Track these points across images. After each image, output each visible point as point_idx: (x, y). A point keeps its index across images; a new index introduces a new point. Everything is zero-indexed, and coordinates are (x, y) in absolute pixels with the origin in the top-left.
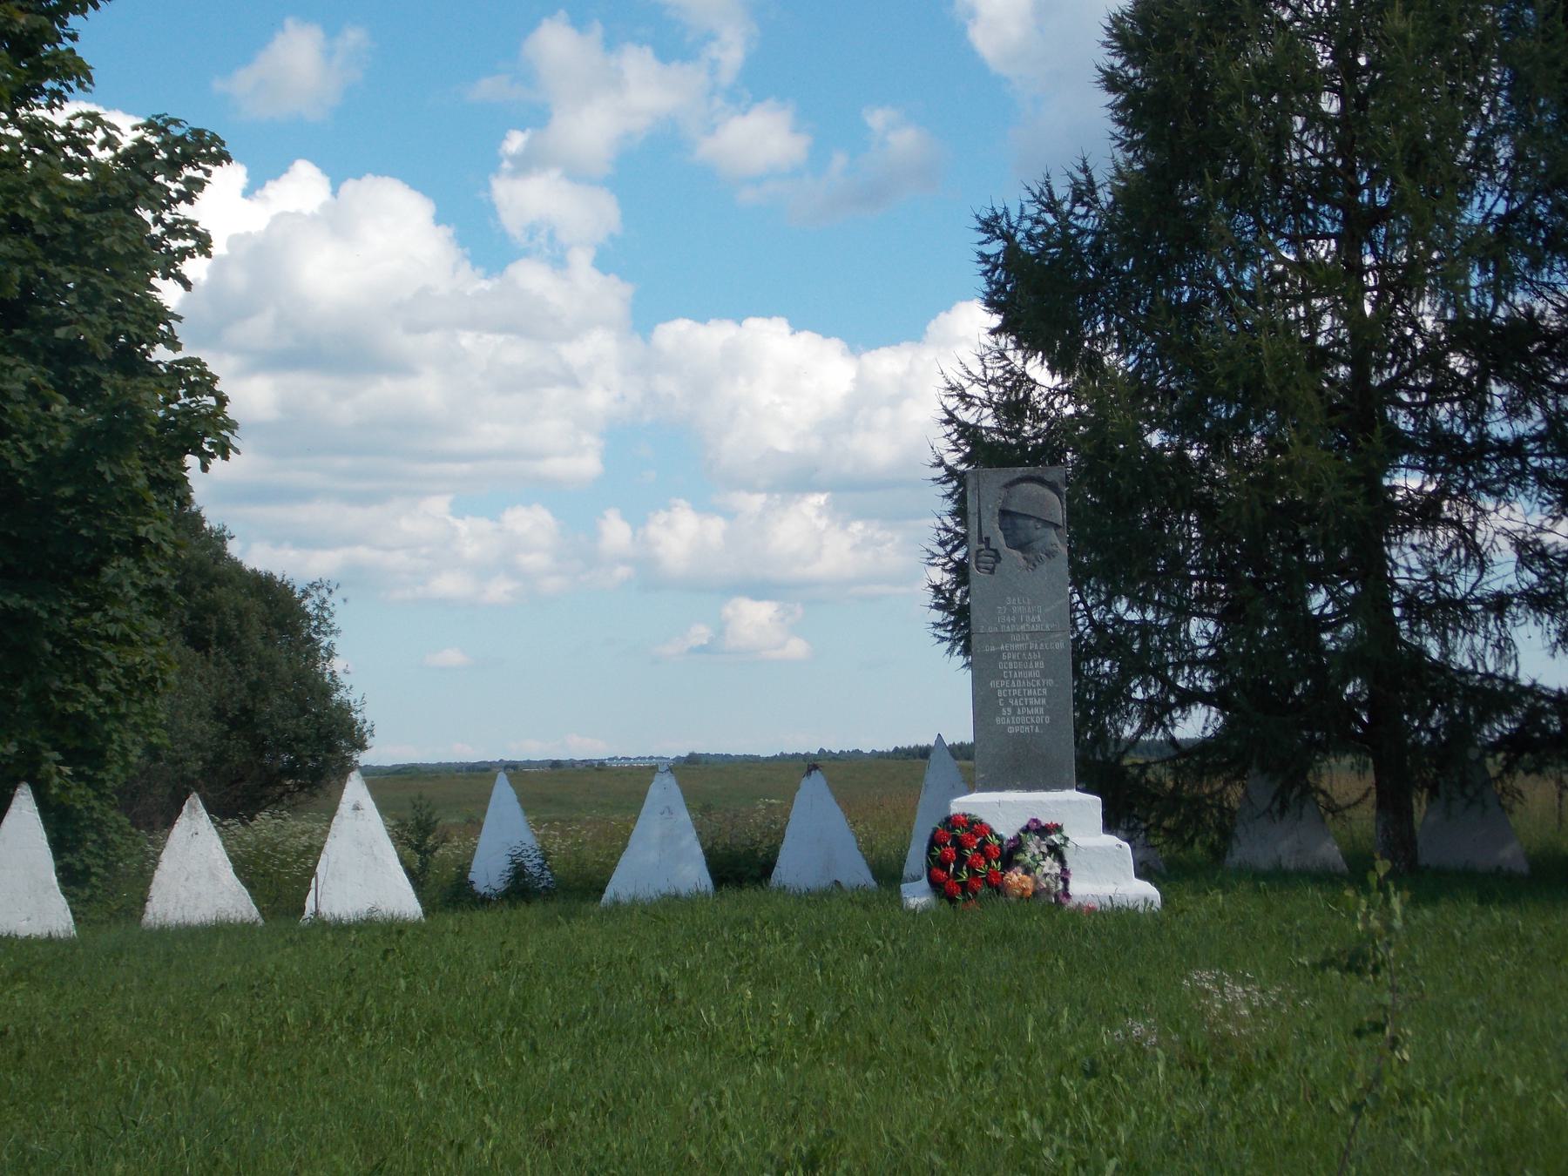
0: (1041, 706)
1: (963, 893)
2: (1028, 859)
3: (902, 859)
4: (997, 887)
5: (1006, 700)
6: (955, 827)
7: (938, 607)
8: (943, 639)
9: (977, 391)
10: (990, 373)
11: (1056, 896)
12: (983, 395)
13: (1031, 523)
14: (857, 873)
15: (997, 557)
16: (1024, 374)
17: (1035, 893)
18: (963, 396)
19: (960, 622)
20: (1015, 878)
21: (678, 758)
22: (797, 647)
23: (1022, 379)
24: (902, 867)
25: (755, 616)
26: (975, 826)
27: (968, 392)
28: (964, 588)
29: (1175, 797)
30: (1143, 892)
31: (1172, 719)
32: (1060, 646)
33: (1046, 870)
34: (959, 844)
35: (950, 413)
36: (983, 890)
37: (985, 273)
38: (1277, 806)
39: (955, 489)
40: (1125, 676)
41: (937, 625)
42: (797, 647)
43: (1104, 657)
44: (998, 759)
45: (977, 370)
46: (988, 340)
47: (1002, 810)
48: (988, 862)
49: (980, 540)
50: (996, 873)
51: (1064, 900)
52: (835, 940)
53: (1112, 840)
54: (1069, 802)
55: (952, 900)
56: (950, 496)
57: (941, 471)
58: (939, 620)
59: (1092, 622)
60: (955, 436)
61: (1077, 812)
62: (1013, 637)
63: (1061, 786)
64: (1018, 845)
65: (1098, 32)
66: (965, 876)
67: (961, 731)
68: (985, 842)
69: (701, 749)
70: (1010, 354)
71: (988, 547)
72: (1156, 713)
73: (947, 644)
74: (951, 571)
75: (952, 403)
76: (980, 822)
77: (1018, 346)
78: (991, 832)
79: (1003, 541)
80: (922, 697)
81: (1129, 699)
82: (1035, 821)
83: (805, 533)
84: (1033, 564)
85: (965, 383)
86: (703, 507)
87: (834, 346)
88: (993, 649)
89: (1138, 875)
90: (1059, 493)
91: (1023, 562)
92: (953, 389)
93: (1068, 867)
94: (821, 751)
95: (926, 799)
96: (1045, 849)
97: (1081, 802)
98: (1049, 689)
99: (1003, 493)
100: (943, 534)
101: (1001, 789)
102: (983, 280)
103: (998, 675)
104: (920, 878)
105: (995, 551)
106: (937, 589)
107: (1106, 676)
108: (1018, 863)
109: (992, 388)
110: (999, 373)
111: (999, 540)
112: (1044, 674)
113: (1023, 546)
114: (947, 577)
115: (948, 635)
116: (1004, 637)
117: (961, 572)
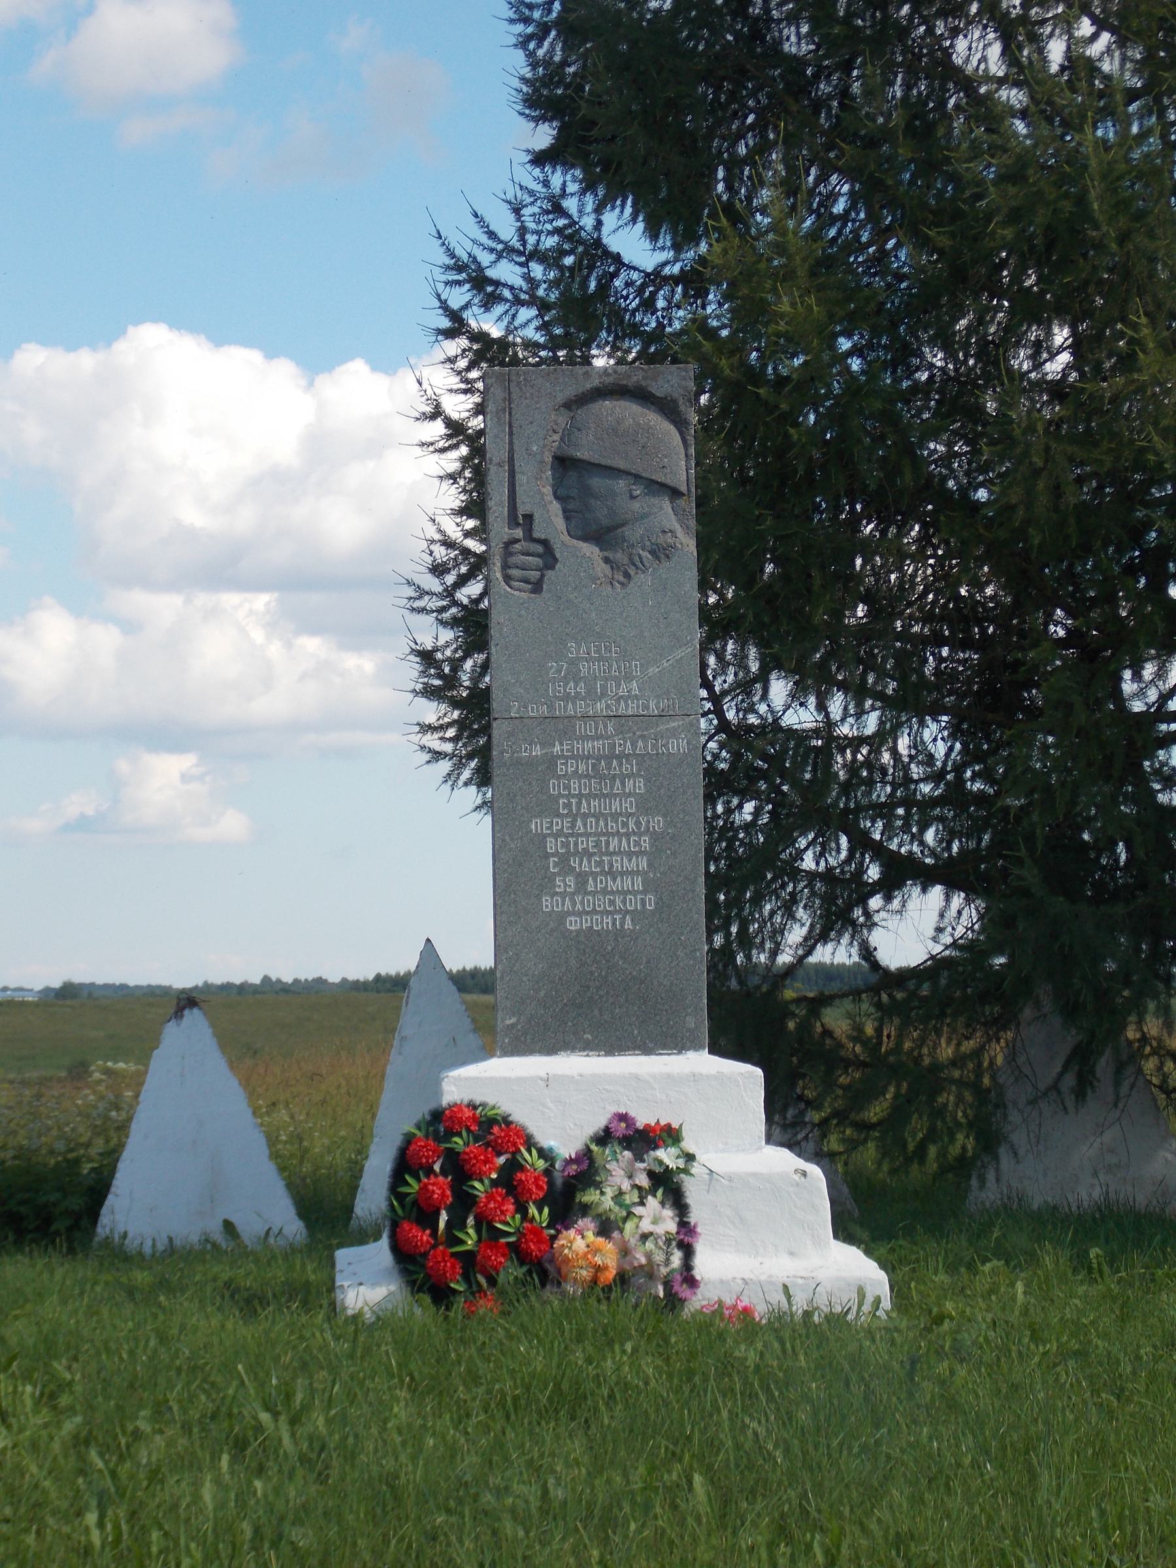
0: (635, 871)
1: (467, 1278)
2: (607, 1202)
3: (356, 1172)
4: (543, 1269)
5: (564, 860)
6: (451, 1133)
7: (429, 692)
8: (437, 756)
9: (508, 272)
10: (531, 239)
11: (667, 1284)
12: (519, 282)
13: (621, 484)
14: (270, 1212)
15: (549, 556)
16: (598, 243)
17: (623, 1278)
18: (480, 281)
19: (473, 721)
20: (580, 1244)
21: (47, 990)
22: (232, 824)
23: (596, 252)
24: (353, 1189)
25: (165, 777)
26: (494, 1131)
27: (491, 273)
28: (480, 658)
29: (879, 1065)
30: (845, 1273)
31: (868, 915)
32: (678, 746)
33: (646, 1226)
34: (460, 1170)
35: (456, 317)
36: (510, 1272)
37: (523, 42)
38: (1070, 1081)
39: (465, 460)
40: (782, 830)
41: (426, 728)
42: (232, 824)
43: (744, 795)
44: (552, 989)
45: (507, 229)
46: (530, 177)
47: (553, 1095)
48: (522, 1209)
49: (513, 521)
50: (537, 1232)
51: (683, 1291)
52: (160, 1410)
53: (783, 1160)
54: (695, 1077)
55: (441, 1295)
56: (453, 477)
57: (438, 429)
58: (431, 719)
59: (724, 725)
60: (462, 363)
61: (713, 1100)
62: (580, 728)
63: (677, 1043)
64: (586, 1171)
65: (470, 1097)
66: (470, 1239)
67: (471, 946)
68: (514, 1165)
69: (83, 974)
70: (571, 204)
71: (529, 537)
72: (842, 905)
73: (445, 766)
74: (454, 623)
75: (458, 297)
76: (507, 1121)
77: (589, 186)
78: (529, 1142)
79: (560, 523)
80: (398, 876)
81: (795, 873)
82: (623, 1117)
83: (240, 651)
84: (623, 573)
85: (485, 258)
86: (82, 605)
87: (284, 370)
88: (537, 751)
89: (844, 1229)
90: (680, 423)
91: (602, 569)
92: (459, 268)
93: (693, 1218)
94: (266, 979)
95: (398, 1064)
96: (643, 1180)
97: (720, 1077)
98: (655, 837)
99: (563, 420)
100: (440, 552)
101: (551, 1050)
102: (519, 57)
103: (549, 808)
104: (377, 1237)
105: (545, 543)
106: (427, 657)
107: (774, 817)
108: (585, 1209)
109: (537, 270)
110: (550, 242)
111: (552, 520)
112: (645, 806)
113: (602, 535)
114: (446, 635)
115: (448, 747)
116: (564, 727)
117: (474, 626)
